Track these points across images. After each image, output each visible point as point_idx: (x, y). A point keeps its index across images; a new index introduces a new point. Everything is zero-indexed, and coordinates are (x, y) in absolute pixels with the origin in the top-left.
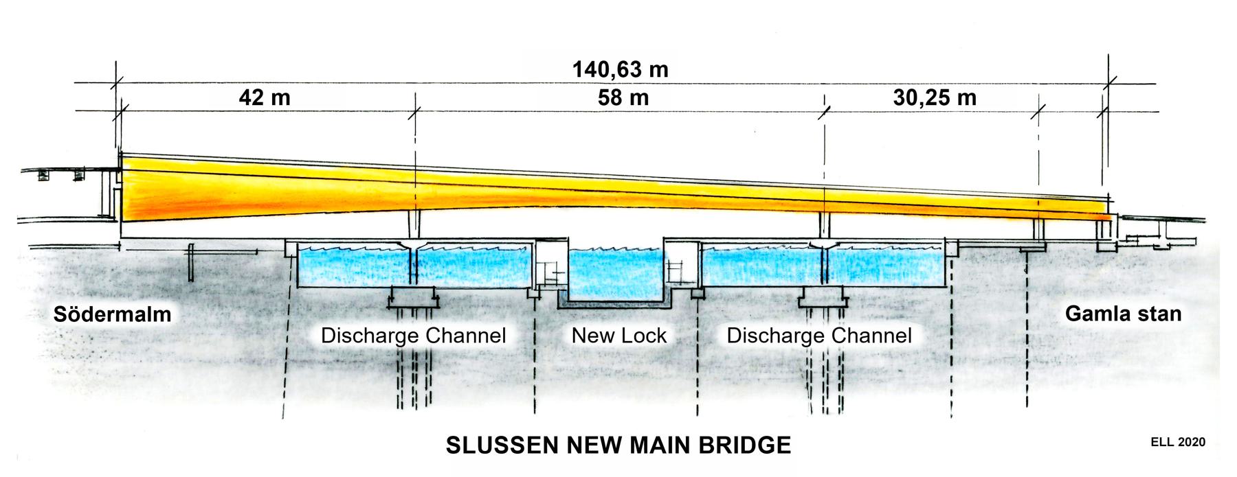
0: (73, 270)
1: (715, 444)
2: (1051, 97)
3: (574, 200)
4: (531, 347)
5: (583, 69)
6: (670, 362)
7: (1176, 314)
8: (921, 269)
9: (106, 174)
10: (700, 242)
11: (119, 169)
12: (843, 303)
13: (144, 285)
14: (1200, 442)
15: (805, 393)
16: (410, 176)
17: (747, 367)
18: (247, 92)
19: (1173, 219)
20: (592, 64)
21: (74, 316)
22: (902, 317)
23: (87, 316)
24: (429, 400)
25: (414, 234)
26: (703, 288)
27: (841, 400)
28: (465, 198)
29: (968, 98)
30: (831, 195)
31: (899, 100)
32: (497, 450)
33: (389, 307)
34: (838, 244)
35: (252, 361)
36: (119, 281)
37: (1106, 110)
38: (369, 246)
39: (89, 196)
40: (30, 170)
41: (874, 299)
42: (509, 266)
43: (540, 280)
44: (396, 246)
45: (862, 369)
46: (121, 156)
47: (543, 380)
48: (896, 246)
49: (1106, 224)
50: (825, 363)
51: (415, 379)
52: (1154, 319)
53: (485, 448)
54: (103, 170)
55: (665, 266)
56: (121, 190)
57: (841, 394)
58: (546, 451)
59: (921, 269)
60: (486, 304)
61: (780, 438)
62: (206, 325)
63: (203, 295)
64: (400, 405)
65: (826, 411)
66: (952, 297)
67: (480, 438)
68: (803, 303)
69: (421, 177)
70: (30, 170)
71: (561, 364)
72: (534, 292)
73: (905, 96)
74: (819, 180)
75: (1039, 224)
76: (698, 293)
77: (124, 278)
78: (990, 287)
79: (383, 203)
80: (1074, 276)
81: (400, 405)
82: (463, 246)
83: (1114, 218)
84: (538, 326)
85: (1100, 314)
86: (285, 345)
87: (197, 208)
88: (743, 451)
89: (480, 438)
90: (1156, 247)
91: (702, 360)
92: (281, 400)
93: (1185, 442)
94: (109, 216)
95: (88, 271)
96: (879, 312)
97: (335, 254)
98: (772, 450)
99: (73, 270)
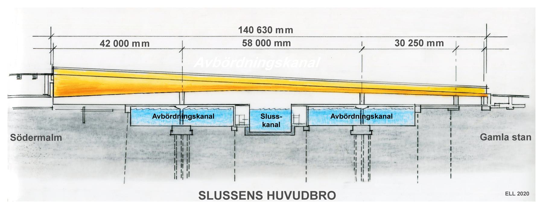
0: (32, 118)
1: (318, 195)
2: (461, 42)
3: (252, 87)
4: (233, 152)
5: (243, 30)
6: (294, 159)
7: (529, 137)
8: (405, 118)
9: (47, 76)
10: (307, 106)
11: (52, 74)
12: (370, 133)
13: (63, 125)
14: (527, 194)
15: (353, 172)
16: (180, 77)
17: (328, 161)
18: (103, 41)
19: (515, 96)
20: (247, 28)
21: (19, 138)
22: (396, 139)
23: (25, 138)
24: (188, 175)
25: (182, 103)
26: (308, 126)
27: (369, 175)
28: (204, 87)
29: (400, 43)
30: (365, 85)
31: (397, 44)
32: (224, 198)
33: (171, 135)
34: (368, 107)
35: (110, 158)
36: (52, 123)
37: (485, 48)
38: (162, 108)
39: (38, 86)
40: (13, 75)
41: (384, 131)
42: (224, 117)
43: (237, 123)
44: (174, 108)
45: (378, 162)
46: (53, 68)
47: (238, 167)
48: (393, 108)
49: (486, 98)
50: (362, 159)
51: (182, 166)
52: (519, 140)
53: (218, 197)
54: (45, 74)
55: (292, 116)
56: (53, 83)
57: (369, 172)
58: (248, 199)
59: (405, 118)
60: (213, 133)
61: (240, 192)
62: (90, 142)
63: (89, 129)
64: (176, 178)
65: (363, 180)
66: (418, 130)
67: (215, 192)
68: (352, 133)
69: (185, 77)
70: (13, 75)
71: (246, 160)
72: (235, 128)
73: (399, 42)
74: (360, 79)
75: (456, 98)
76: (306, 128)
77: (55, 121)
78: (435, 126)
79: (168, 89)
80: (472, 122)
81: (176, 178)
82: (203, 108)
83: (489, 96)
84: (236, 143)
85: (495, 137)
86: (125, 151)
87: (86, 91)
88: (303, 199)
89: (215, 192)
90: (507, 108)
91: (308, 158)
92: (123, 176)
93: (520, 194)
94: (48, 95)
95: (39, 119)
96: (386, 137)
97: (147, 111)
98: (204, 198)
99: (32, 118)
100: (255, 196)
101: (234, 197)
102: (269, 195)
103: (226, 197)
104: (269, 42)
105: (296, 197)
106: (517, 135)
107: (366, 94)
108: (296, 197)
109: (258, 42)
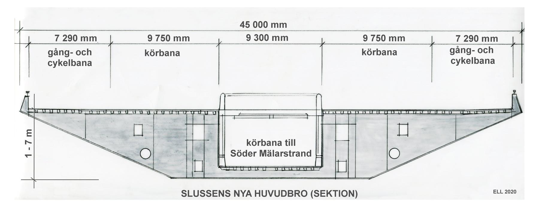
1: (294, 193)
14: (514, 192)
21: (239, 154)
23: (245, 154)
31: (256, 39)
52: (290, 156)
53: (196, 194)
54: (386, 112)
73: (258, 37)
88: (282, 196)
93: (507, 192)
100: (225, 194)
101: (209, 195)
102: (256, 193)
103: (203, 195)
104: (255, 26)
105: (277, 194)
106: (288, 151)
108: (277, 194)
109: (266, 26)
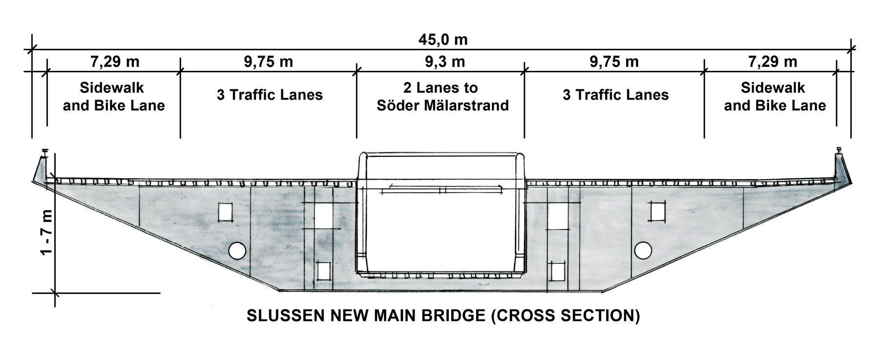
1: (433, 315)
21: (391, 107)
53: (274, 317)
61: (574, 311)
67: (270, 311)
88: (453, 320)
89: (270, 311)
98: (255, 320)
101: (297, 318)
107: (221, 206)
